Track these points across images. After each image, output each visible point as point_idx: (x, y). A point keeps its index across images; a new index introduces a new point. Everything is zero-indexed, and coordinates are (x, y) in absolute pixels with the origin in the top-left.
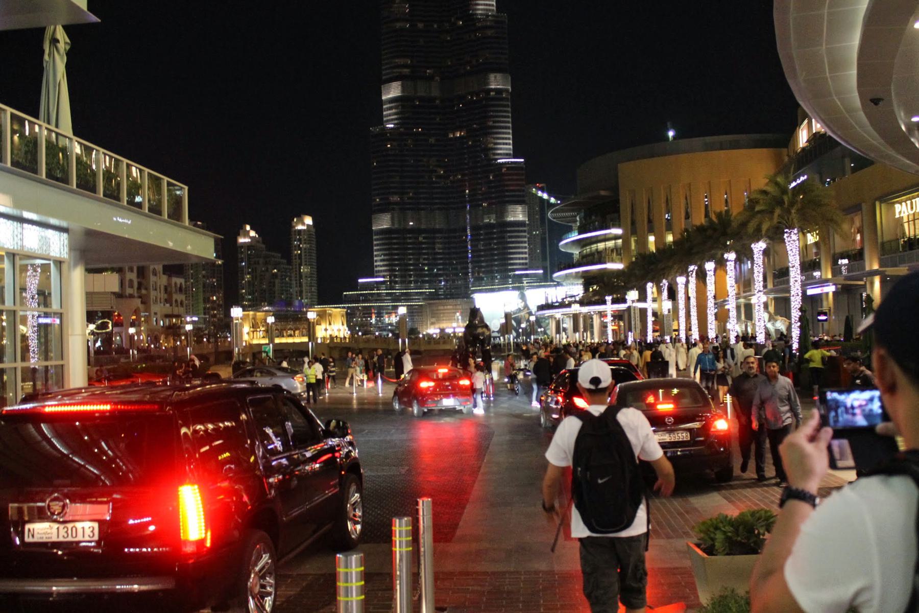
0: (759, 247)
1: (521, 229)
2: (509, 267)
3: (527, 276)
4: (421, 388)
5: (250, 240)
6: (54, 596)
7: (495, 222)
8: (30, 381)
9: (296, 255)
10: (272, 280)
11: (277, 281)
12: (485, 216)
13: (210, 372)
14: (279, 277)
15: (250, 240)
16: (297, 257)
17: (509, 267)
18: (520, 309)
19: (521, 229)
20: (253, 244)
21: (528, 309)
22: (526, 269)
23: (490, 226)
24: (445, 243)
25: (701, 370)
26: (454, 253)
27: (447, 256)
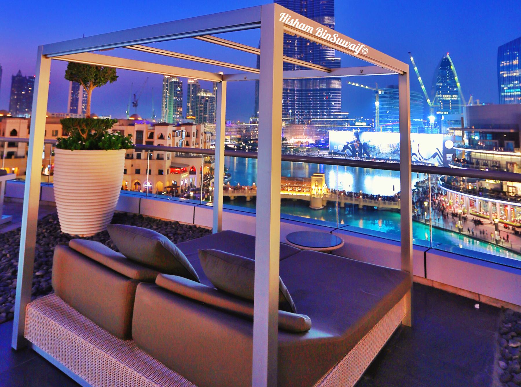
0: (423, 104)
1: (338, 92)
2: (332, 110)
3: (340, 115)
4: (424, 203)
5: (194, 82)
6: (490, 376)
7: (325, 88)
8: (245, 160)
9: (215, 90)
10: (206, 103)
11: (208, 103)
12: (321, 85)
13: (448, 176)
14: (209, 101)
15: (194, 82)
16: (216, 91)
17: (332, 110)
18: (354, 141)
19: (338, 92)
20: (195, 83)
21: (360, 141)
22: (340, 112)
23: (323, 90)
24: (300, 96)
25: (306, 232)
26: (304, 99)
27: (300, 100)
